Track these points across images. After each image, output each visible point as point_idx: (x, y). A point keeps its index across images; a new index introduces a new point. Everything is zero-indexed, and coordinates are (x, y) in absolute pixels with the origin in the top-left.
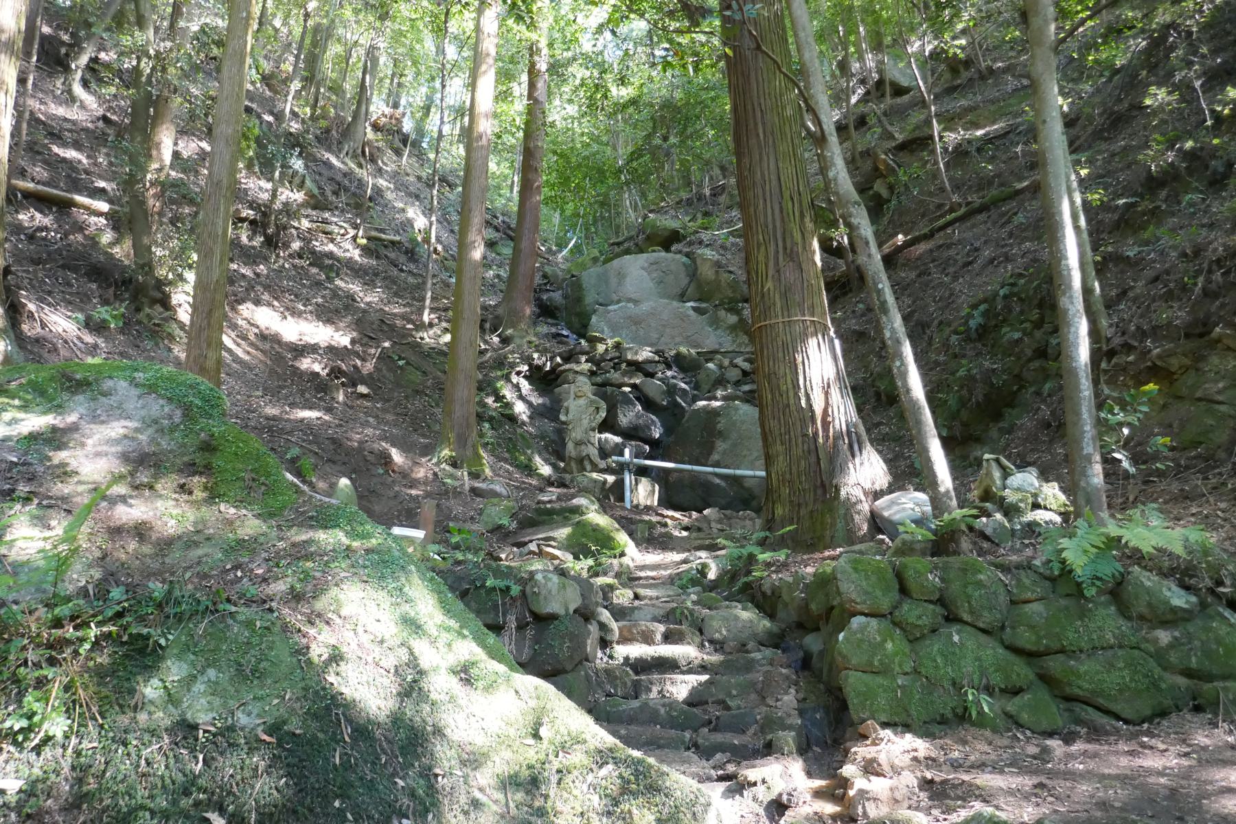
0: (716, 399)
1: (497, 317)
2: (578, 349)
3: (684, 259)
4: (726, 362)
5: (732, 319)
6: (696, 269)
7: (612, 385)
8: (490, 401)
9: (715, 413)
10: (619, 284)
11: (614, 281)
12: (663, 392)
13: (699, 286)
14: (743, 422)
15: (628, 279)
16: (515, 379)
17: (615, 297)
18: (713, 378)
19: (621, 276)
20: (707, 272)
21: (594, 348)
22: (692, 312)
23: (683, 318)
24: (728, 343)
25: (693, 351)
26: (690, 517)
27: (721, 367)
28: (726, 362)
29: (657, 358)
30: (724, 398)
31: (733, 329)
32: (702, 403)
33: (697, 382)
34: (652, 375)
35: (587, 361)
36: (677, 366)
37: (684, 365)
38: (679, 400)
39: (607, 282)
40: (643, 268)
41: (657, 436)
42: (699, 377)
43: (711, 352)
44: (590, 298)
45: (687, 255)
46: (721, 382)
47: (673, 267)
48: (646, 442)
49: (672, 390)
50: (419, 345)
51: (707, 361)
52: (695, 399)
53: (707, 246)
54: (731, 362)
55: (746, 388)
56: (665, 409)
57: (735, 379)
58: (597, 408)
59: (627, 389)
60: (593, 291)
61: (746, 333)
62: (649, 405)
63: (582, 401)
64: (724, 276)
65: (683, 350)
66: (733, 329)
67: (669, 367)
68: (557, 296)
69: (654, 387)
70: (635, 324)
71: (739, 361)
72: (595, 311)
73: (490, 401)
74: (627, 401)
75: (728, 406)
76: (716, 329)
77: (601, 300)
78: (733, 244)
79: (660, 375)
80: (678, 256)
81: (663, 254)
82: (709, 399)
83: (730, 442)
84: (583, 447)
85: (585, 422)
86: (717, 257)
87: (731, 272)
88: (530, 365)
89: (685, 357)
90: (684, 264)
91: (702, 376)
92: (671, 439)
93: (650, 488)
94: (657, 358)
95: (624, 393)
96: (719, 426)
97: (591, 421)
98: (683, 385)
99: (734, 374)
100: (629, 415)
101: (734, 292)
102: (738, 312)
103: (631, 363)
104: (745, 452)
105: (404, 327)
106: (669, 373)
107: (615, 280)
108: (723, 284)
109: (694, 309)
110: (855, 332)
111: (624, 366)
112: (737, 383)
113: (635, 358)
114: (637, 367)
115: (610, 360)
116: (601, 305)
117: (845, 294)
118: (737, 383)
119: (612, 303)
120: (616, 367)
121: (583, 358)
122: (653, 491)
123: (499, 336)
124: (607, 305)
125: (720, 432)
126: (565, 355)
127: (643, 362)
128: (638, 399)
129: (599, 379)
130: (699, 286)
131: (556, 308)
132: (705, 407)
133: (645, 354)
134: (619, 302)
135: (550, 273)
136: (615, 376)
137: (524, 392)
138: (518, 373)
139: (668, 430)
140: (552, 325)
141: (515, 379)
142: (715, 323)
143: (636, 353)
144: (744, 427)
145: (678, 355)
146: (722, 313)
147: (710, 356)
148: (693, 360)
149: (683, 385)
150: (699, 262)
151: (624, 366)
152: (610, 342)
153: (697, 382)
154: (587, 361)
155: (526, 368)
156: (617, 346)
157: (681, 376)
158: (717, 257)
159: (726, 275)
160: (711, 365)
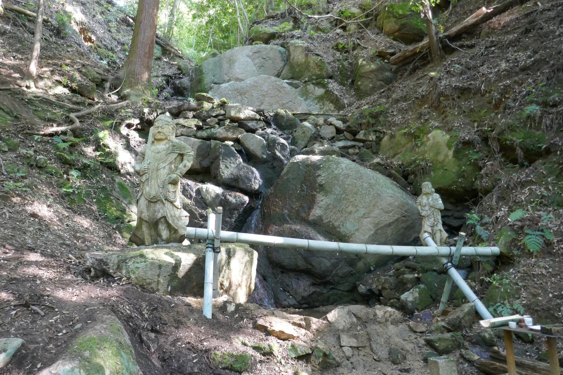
0: (313, 153)
1: (117, 78)
2: (186, 106)
3: (281, 48)
4: (321, 121)
5: (320, 91)
6: (290, 55)
7: (216, 139)
8: (89, 150)
9: (315, 166)
10: (230, 68)
11: (225, 66)
12: (263, 147)
13: (292, 67)
14: (347, 176)
15: (236, 64)
16: (124, 130)
17: (226, 78)
18: (309, 135)
19: (231, 62)
20: (298, 57)
21: (200, 105)
22: (287, 85)
23: (279, 89)
24: (315, 109)
25: (290, 113)
26: (308, 327)
27: (316, 125)
28: (321, 121)
29: (258, 117)
30: (322, 153)
31: (320, 99)
32: (300, 157)
33: (294, 139)
34: (253, 131)
35: (194, 117)
36: (275, 125)
37: (283, 124)
38: (278, 154)
39: (221, 67)
40: (248, 56)
41: (257, 187)
42: (295, 134)
43: (306, 114)
44: (208, 79)
45: (282, 46)
46: (317, 137)
47: (271, 55)
48: (245, 192)
49: (271, 144)
50: (23, 93)
51: (302, 121)
52: (293, 153)
53: (298, 38)
54: (325, 121)
55: (341, 144)
56: (265, 162)
57: (329, 136)
58: (182, 155)
59: (230, 143)
60: (210, 74)
61: (332, 102)
62: (249, 157)
63: (161, 146)
64: (313, 59)
65: (282, 111)
66: (320, 99)
67: (268, 124)
68: (186, 81)
69: (255, 142)
70: (241, 95)
71: (332, 120)
72: (211, 88)
73: (89, 150)
74: (229, 154)
75: (328, 160)
76: (305, 100)
77: (216, 80)
78: (318, 37)
79: (260, 131)
80: (276, 46)
81: (264, 45)
82: (307, 153)
83: (333, 197)
84: (158, 206)
85: (163, 173)
86: (306, 44)
87: (318, 55)
88: (141, 119)
89: (283, 117)
90: (280, 52)
91: (298, 133)
92: (271, 190)
93: (247, 258)
94: (258, 117)
95: (227, 146)
96: (319, 180)
97: (171, 172)
98: (283, 141)
99: (328, 132)
100: (229, 168)
101: (321, 70)
102: (324, 86)
103: (233, 120)
104: (350, 208)
105: (9, 76)
106: (269, 130)
107: (227, 65)
108: (312, 64)
109: (287, 83)
110: (456, 88)
111: (227, 122)
112: (332, 140)
113: (238, 115)
114: (240, 123)
115: (216, 116)
116: (215, 83)
117: (424, 65)
118: (332, 140)
119: (224, 82)
120: (220, 123)
121: (191, 114)
122: (251, 262)
123: (118, 93)
124: (220, 84)
125: (321, 186)
126: (174, 111)
127: (244, 120)
128: (239, 152)
129: (204, 134)
130: (292, 67)
131: (185, 89)
132: (303, 162)
133: (247, 112)
134: (229, 81)
135: (183, 66)
136: (219, 131)
137: (133, 143)
138: (129, 126)
139: (268, 181)
140: (181, 100)
141: (124, 130)
142: (305, 94)
143: (239, 111)
144: (348, 181)
145: (277, 115)
146: (311, 87)
147: (304, 117)
148: (289, 120)
149: (283, 141)
150: (291, 49)
151: (227, 122)
152: (217, 102)
153: (294, 139)
154: (194, 117)
155: (137, 121)
156: (223, 105)
157: (280, 133)
158: (306, 44)
159: (315, 57)
160: (306, 124)
